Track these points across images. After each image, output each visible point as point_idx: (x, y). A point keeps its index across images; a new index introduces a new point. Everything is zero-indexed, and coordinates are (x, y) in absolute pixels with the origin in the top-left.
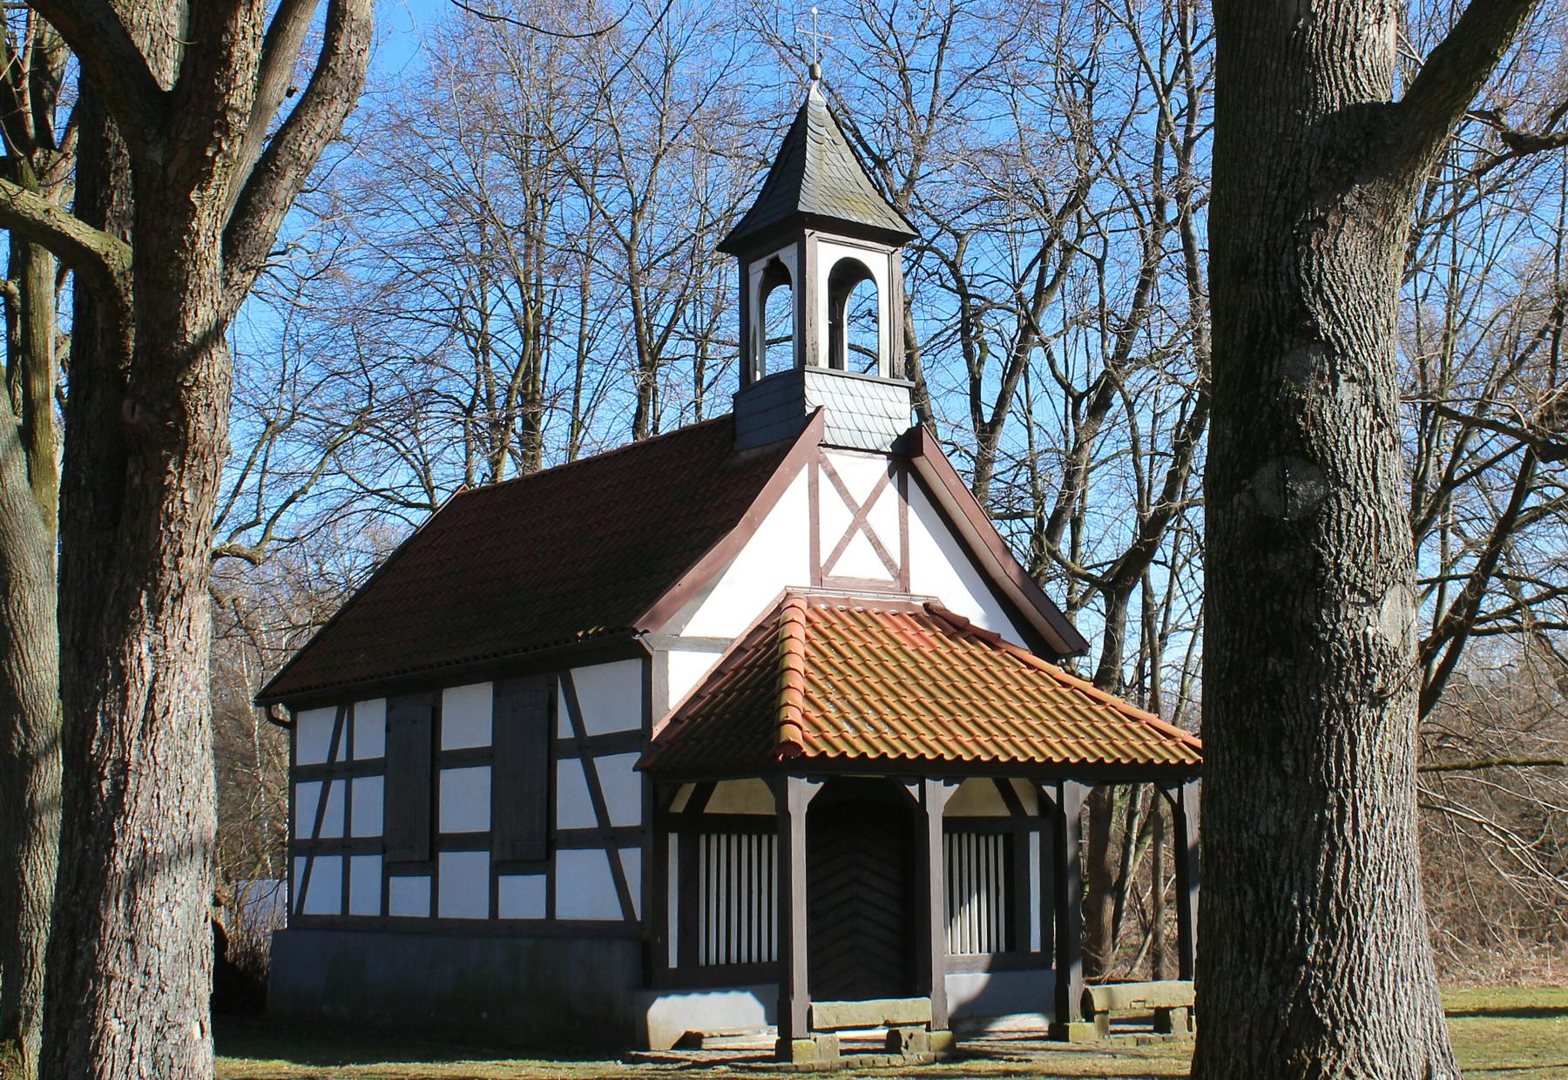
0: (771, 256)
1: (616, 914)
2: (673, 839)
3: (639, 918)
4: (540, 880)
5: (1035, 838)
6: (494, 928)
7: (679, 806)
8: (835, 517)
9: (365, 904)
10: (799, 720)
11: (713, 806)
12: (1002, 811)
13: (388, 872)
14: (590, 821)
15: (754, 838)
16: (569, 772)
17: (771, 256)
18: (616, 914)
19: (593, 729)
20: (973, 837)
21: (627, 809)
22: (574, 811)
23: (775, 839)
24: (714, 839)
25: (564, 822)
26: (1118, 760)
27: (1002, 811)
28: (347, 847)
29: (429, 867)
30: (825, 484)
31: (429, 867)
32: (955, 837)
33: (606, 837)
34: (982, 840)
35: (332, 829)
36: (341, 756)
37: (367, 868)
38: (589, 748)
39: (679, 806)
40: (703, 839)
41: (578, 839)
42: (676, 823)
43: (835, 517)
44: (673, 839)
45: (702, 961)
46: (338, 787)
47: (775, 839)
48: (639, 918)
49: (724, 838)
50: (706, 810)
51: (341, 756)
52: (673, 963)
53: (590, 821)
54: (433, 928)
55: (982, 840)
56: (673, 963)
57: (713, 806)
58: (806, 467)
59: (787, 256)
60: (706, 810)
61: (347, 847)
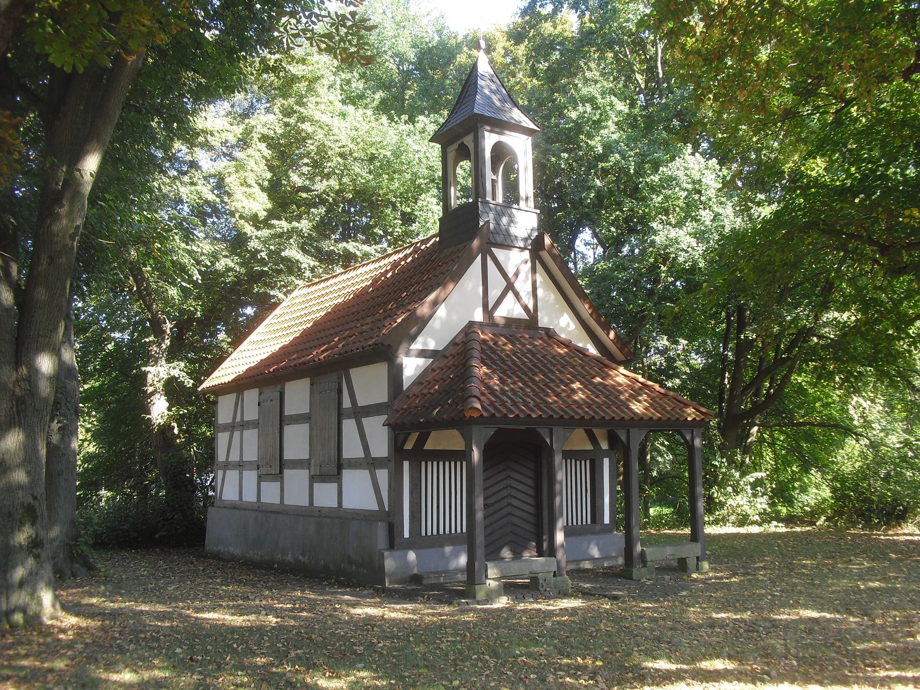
0: (459, 142)
1: (375, 507)
2: (406, 464)
3: (387, 510)
4: (334, 486)
5: (606, 462)
6: (311, 513)
7: (409, 446)
8: (497, 285)
9: (250, 496)
10: (478, 394)
11: (429, 446)
12: (590, 447)
13: (260, 478)
14: (360, 454)
15: (453, 463)
16: (349, 426)
17: (459, 142)
18: (375, 507)
19: (361, 403)
20: (573, 461)
21: (380, 447)
22: (352, 449)
23: (464, 463)
24: (430, 464)
25: (347, 454)
26: (573, 417)
27: (590, 447)
28: (241, 466)
29: (279, 476)
30: (490, 263)
31: (279, 476)
32: (569, 461)
33: (370, 463)
34: (578, 462)
35: (234, 457)
36: (238, 419)
37: (251, 477)
38: (359, 413)
39: (409, 446)
40: (423, 464)
41: (354, 464)
42: (408, 455)
43: (497, 285)
44: (406, 464)
45: (423, 534)
46: (237, 434)
47: (464, 463)
48: (387, 510)
49: (435, 463)
50: (425, 448)
51: (238, 419)
52: (406, 535)
53: (360, 454)
54: (281, 512)
55: (578, 462)
56: (406, 535)
57: (429, 446)
58: (479, 257)
59: (468, 140)
60: (425, 448)
61: (241, 466)
